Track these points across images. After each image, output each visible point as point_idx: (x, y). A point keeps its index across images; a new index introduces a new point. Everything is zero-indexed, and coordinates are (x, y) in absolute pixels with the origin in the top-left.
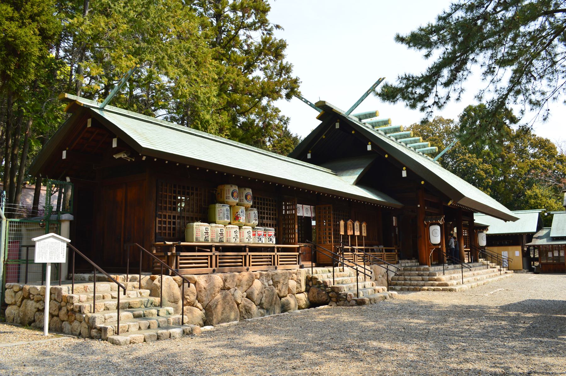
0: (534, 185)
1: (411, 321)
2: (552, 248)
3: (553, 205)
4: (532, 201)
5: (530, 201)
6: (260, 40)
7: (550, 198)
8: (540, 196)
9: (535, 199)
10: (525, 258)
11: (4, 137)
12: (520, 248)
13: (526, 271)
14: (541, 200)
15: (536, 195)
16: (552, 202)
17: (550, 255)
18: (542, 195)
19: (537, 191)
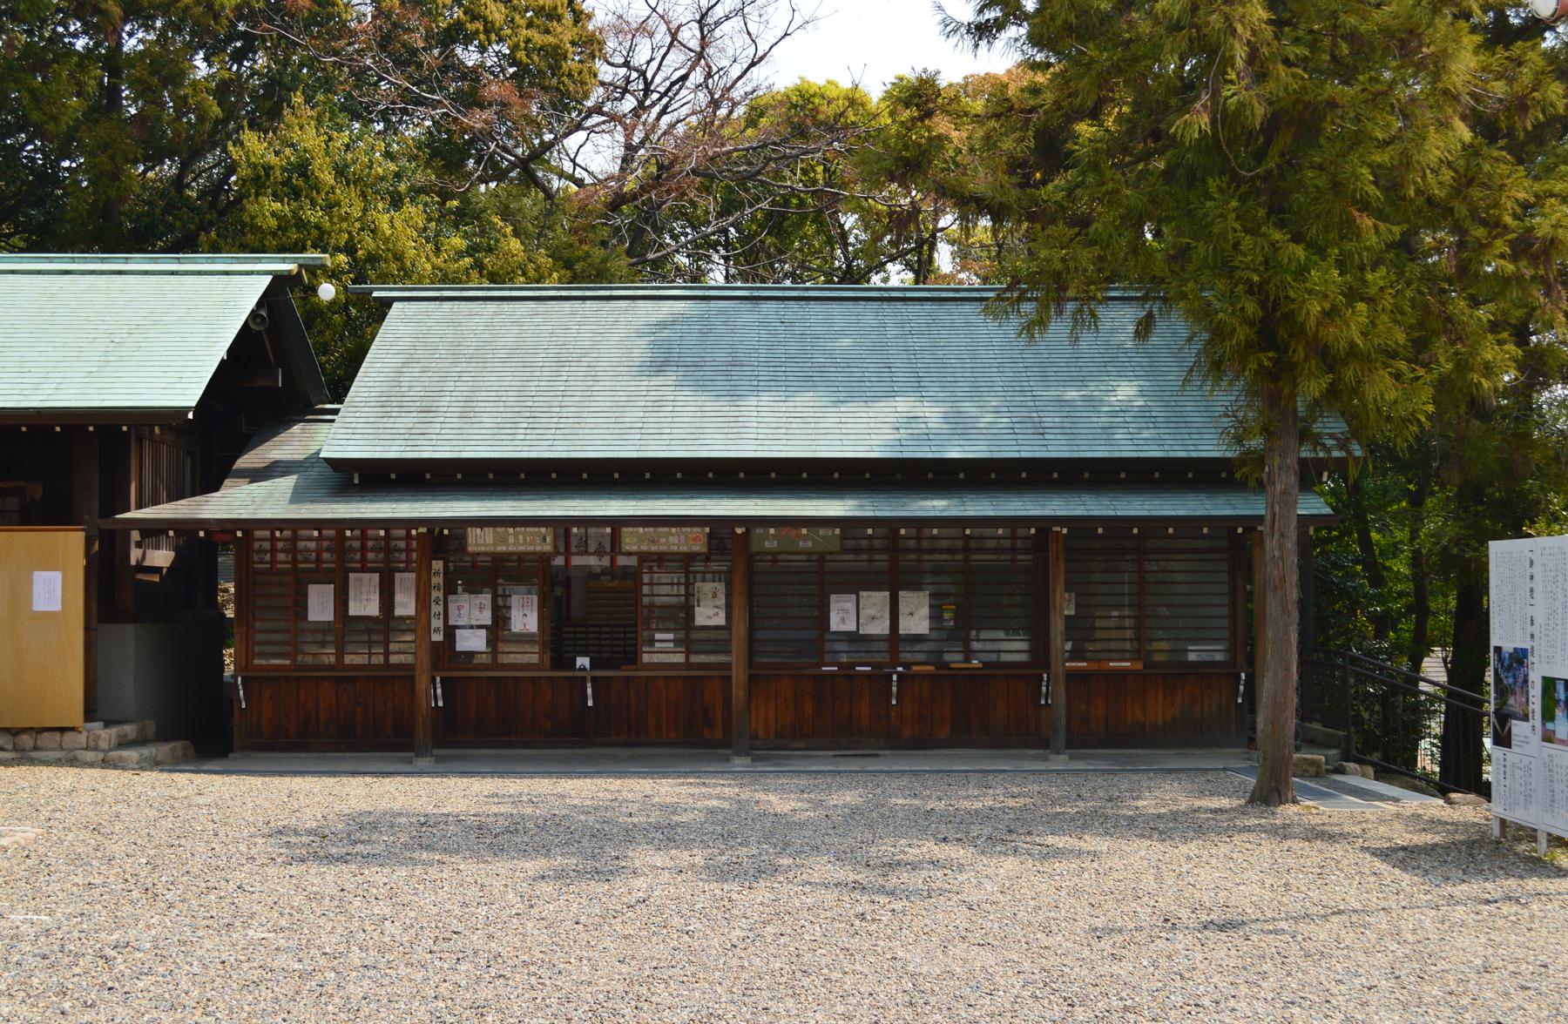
0: (298, 99)
1: (1198, 803)
2: (343, 551)
3: (409, 248)
4: (268, 209)
5: (252, 208)
6: (1052, 326)
7: (396, 202)
8: (328, 178)
9: (296, 194)
10: (126, 640)
11: (1000, 531)
12: (71, 543)
13: (106, 735)
14: (330, 207)
15: (302, 168)
16: (400, 227)
17: (320, 606)
18: (340, 171)
19: (310, 139)
